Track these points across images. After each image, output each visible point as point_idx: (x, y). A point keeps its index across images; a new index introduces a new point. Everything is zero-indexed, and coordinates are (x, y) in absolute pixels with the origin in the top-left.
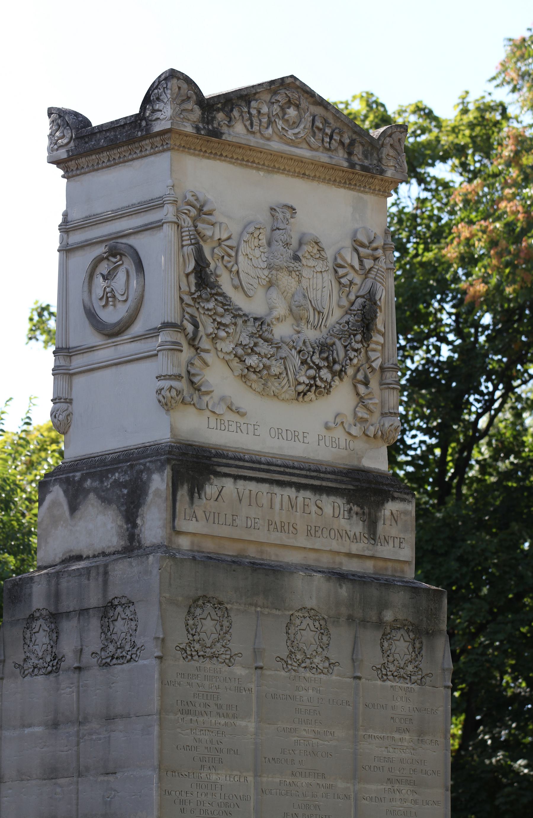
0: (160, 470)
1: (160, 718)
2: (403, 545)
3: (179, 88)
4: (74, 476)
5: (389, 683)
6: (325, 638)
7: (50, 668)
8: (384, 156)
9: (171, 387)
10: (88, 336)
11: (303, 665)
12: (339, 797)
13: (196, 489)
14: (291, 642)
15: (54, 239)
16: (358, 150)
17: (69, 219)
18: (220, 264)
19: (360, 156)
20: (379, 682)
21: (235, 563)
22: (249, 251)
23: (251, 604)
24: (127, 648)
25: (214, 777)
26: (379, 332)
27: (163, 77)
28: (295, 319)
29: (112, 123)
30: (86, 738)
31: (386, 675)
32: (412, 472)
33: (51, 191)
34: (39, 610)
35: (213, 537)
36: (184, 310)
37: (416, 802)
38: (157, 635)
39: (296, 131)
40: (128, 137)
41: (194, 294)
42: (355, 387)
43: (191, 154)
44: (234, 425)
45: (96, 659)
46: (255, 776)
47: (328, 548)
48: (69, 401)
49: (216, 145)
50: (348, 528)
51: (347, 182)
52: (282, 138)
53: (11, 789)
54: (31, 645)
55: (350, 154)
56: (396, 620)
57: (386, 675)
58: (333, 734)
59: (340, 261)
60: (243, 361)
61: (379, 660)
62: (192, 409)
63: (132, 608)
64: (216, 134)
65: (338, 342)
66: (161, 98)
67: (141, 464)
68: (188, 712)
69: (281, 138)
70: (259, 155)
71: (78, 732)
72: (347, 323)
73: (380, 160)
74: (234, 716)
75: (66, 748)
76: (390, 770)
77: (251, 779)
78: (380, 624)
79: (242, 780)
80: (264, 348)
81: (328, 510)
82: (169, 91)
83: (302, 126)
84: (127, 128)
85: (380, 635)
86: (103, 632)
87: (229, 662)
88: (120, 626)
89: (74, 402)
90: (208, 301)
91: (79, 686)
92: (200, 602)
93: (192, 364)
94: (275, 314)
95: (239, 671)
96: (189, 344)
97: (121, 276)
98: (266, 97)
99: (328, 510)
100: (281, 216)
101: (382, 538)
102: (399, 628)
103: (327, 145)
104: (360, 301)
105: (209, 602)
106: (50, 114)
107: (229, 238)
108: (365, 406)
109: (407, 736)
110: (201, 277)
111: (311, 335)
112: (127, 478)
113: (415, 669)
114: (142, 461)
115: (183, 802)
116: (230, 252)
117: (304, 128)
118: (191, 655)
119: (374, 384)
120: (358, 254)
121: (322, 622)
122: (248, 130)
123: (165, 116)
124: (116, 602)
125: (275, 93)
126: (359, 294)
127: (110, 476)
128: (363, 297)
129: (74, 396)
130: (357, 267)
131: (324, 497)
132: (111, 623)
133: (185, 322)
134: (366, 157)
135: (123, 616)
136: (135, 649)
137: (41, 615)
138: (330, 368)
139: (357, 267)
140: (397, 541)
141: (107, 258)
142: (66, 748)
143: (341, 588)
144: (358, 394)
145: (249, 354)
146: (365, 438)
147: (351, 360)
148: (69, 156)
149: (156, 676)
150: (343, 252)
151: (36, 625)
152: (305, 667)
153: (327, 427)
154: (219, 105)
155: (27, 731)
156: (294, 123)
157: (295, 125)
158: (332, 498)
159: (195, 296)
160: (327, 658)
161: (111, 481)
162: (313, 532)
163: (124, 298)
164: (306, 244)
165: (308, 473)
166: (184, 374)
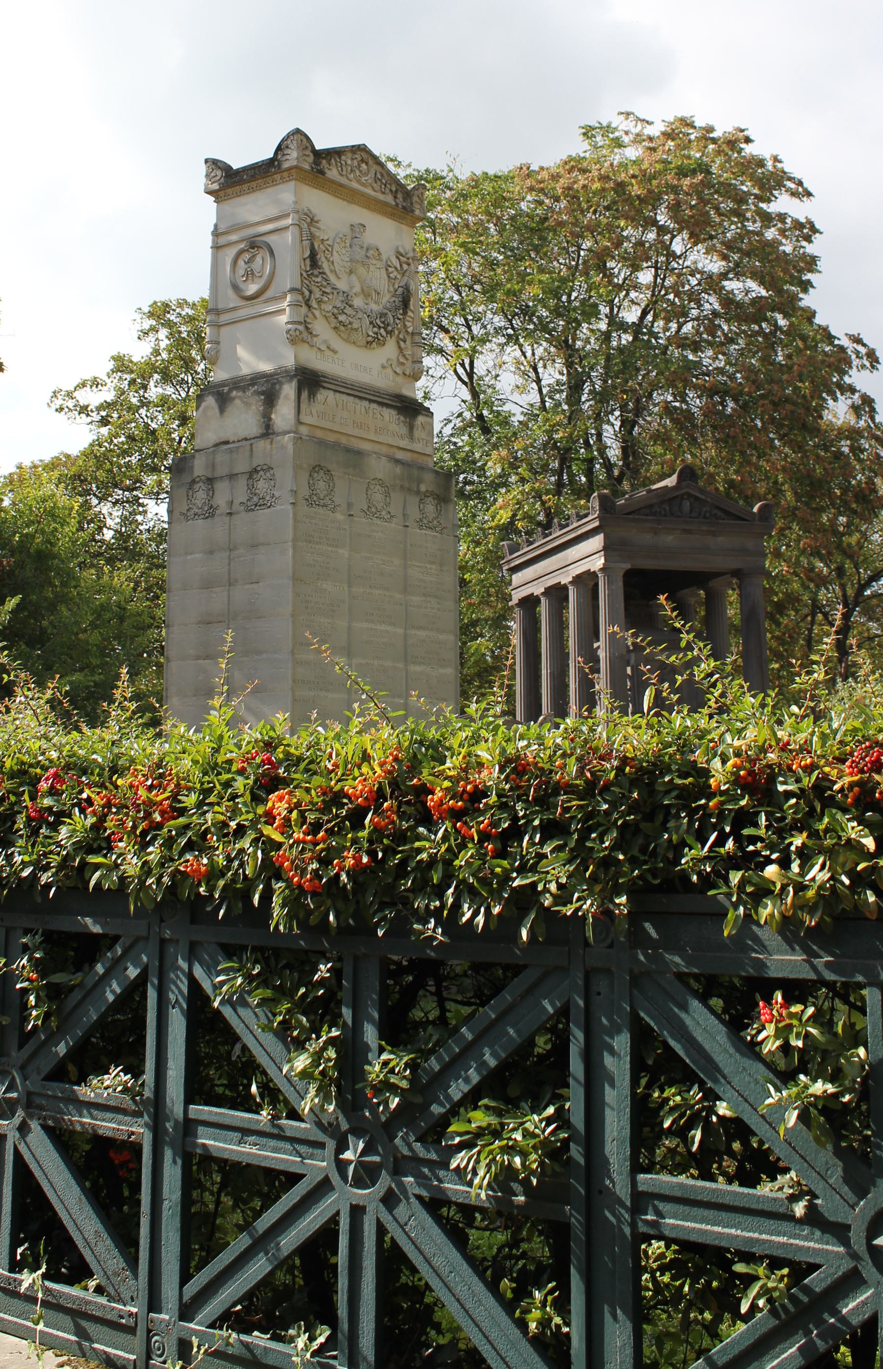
10: (232, 300)
13: (312, 395)
15: (209, 240)
16: (400, 196)
21: (336, 445)
25: (325, 586)
37: (439, 610)
46: (349, 586)
48: (218, 343)
51: (392, 216)
52: (359, 181)
55: (395, 197)
60: (336, 318)
61: (418, 516)
62: (306, 345)
64: (322, 172)
68: (310, 542)
74: (337, 547)
78: (418, 492)
80: (349, 311)
81: (387, 417)
90: (317, 276)
94: (354, 291)
95: (340, 517)
97: (259, 259)
98: (349, 155)
106: (206, 161)
108: (404, 356)
109: (434, 567)
111: (375, 307)
115: (307, 602)
116: (330, 249)
119: (408, 342)
123: (292, 157)
138: (385, 329)
144: (400, 347)
155: (189, 557)
157: (366, 174)
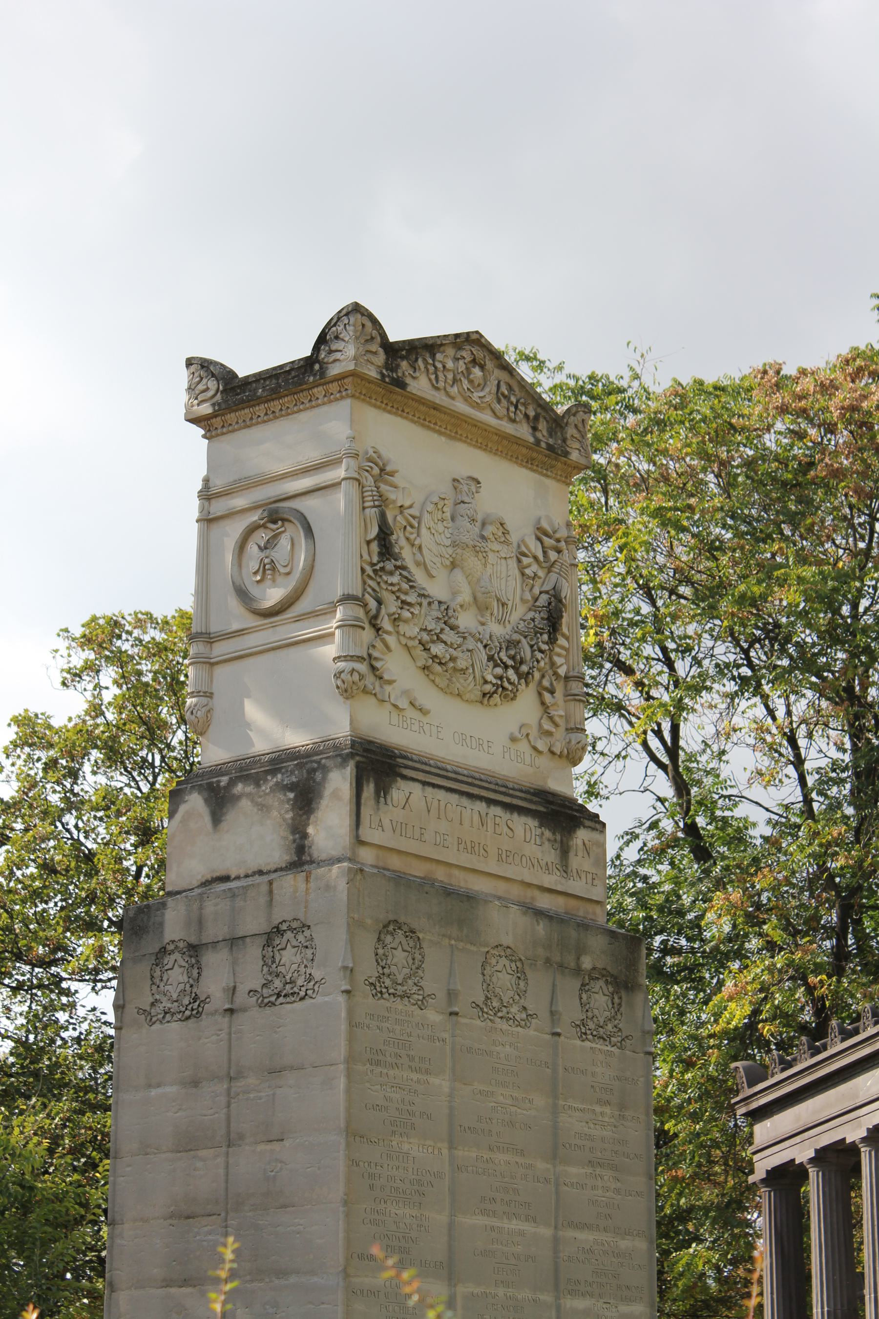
0: (343, 764)
1: (348, 1068)
2: (595, 882)
3: (363, 325)
4: (219, 782)
5: (587, 1044)
6: (522, 983)
7: (188, 1013)
8: (568, 436)
9: (353, 670)
10: (235, 616)
11: (500, 1014)
12: (539, 1181)
13: (382, 791)
14: (487, 985)
16: (542, 425)
17: (211, 484)
18: (401, 535)
19: (545, 433)
20: (578, 1042)
21: (425, 885)
22: (432, 524)
24: (300, 982)
25: (406, 1147)
26: (564, 635)
27: (344, 312)
28: (479, 608)
29: (274, 369)
30: (241, 1097)
31: (585, 1034)
33: (189, 455)
34: (173, 941)
35: (399, 852)
36: (364, 583)
37: (617, 1191)
38: (345, 964)
39: (481, 394)
40: (292, 384)
41: (375, 565)
42: (540, 694)
43: (370, 404)
44: (417, 723)
45: (255, 998)
46: (451, 1148)
47: (519, 879)
48: (209, 695)
49: (399, 398)
50: (540, 856)
51: (529, 463)
52: (467, 400)
53: (129, 1166)
54: (162, 984)
55: (535, 429)
56: (594, 969)
57: (585, 1034)
58: (531, 1101)
59: (524, 549)
60: (426, 650)
61: (578, 1015)
62: (372, 700)
63: (307, 933)
64: (400, 384)
65: (524, 640)
66: (341, 336)
67: (314, 761)
68: (378, 1063)
69: (466, 400)
70: (442, 416)
71: (229, 1090)
72: (533, 620)
73: (564, 440)
74: (427, 1072)
75: (210, 1112)
76: (591, 1150)
77: (445, 1151)
78: (578, 971)
79: (436, 1152)
80: (449, 636)
81: (519, 831)
82: (352, 328)
83: (487, 390)
84: (293, 374)
85: (577, 984)
86: (265, 964)
88: (289, 958)
89: (215, 696)
90: (391, 573)
91: (230, 1034)
92: (391, 928)
93: (374, 646)
95: (433, 1016)
96: (370, 623)
97: (284, 542)
98: (451, 351)
99: (519, 831)
100: (465, 488)
101: (575, 871)
102: (598, 979)
103: (512, 415)
104: (544, 598)
105: (400, 928)
106: (189, 363)
107: (411, 507)
108: (551, 718)
109: (607, 1110)
110: (385, 546)
111: (498, 630)
112: (294, 779)
113: (615, 1030)
114: (315, 758)
115: (371, 1176)
116: (414, 524)
117: (490, 393)
118: (381, 992)
119: (559, 694)
120: (542, 543)
121: (519, 964)
122: (433, 385)
123: (346, 355)
124: (284, 927)
125: (459, 348)
126: (543, 589)
127: (269, 778)
128: (547, 592)
129: (214, 690)
130: (541, 558)
131: (515, 815)
132: (276, 952)
133: (367, 596)
134: (551, 436)
135: (295, 943)
136: (312, 983)
137: (176, 947)
138: (516, 669)
139: (541, 558)
140: (590, 876)
141: (264, 526)
142: (210, 1112)
143: (538, 924)
144: (543, 703)
145: (433, 642)
146: (550, 755)
147: (538, 661)
148: (215, 411)
149: (343, 1014)
150: (527, 539)
151: (169, 960)
152: (501, 1018)
153: (513, 739)
154: (404, 353)
155: (154, 1092)
156: (479, 385)
158: (524, 819)
159: (378, 567)
160: (524, 1008)
161: (271, 784)
162: (504, 856)
163: (287, 570)
164: (491, 524)
165: (497, 788)
166: (365, 656)
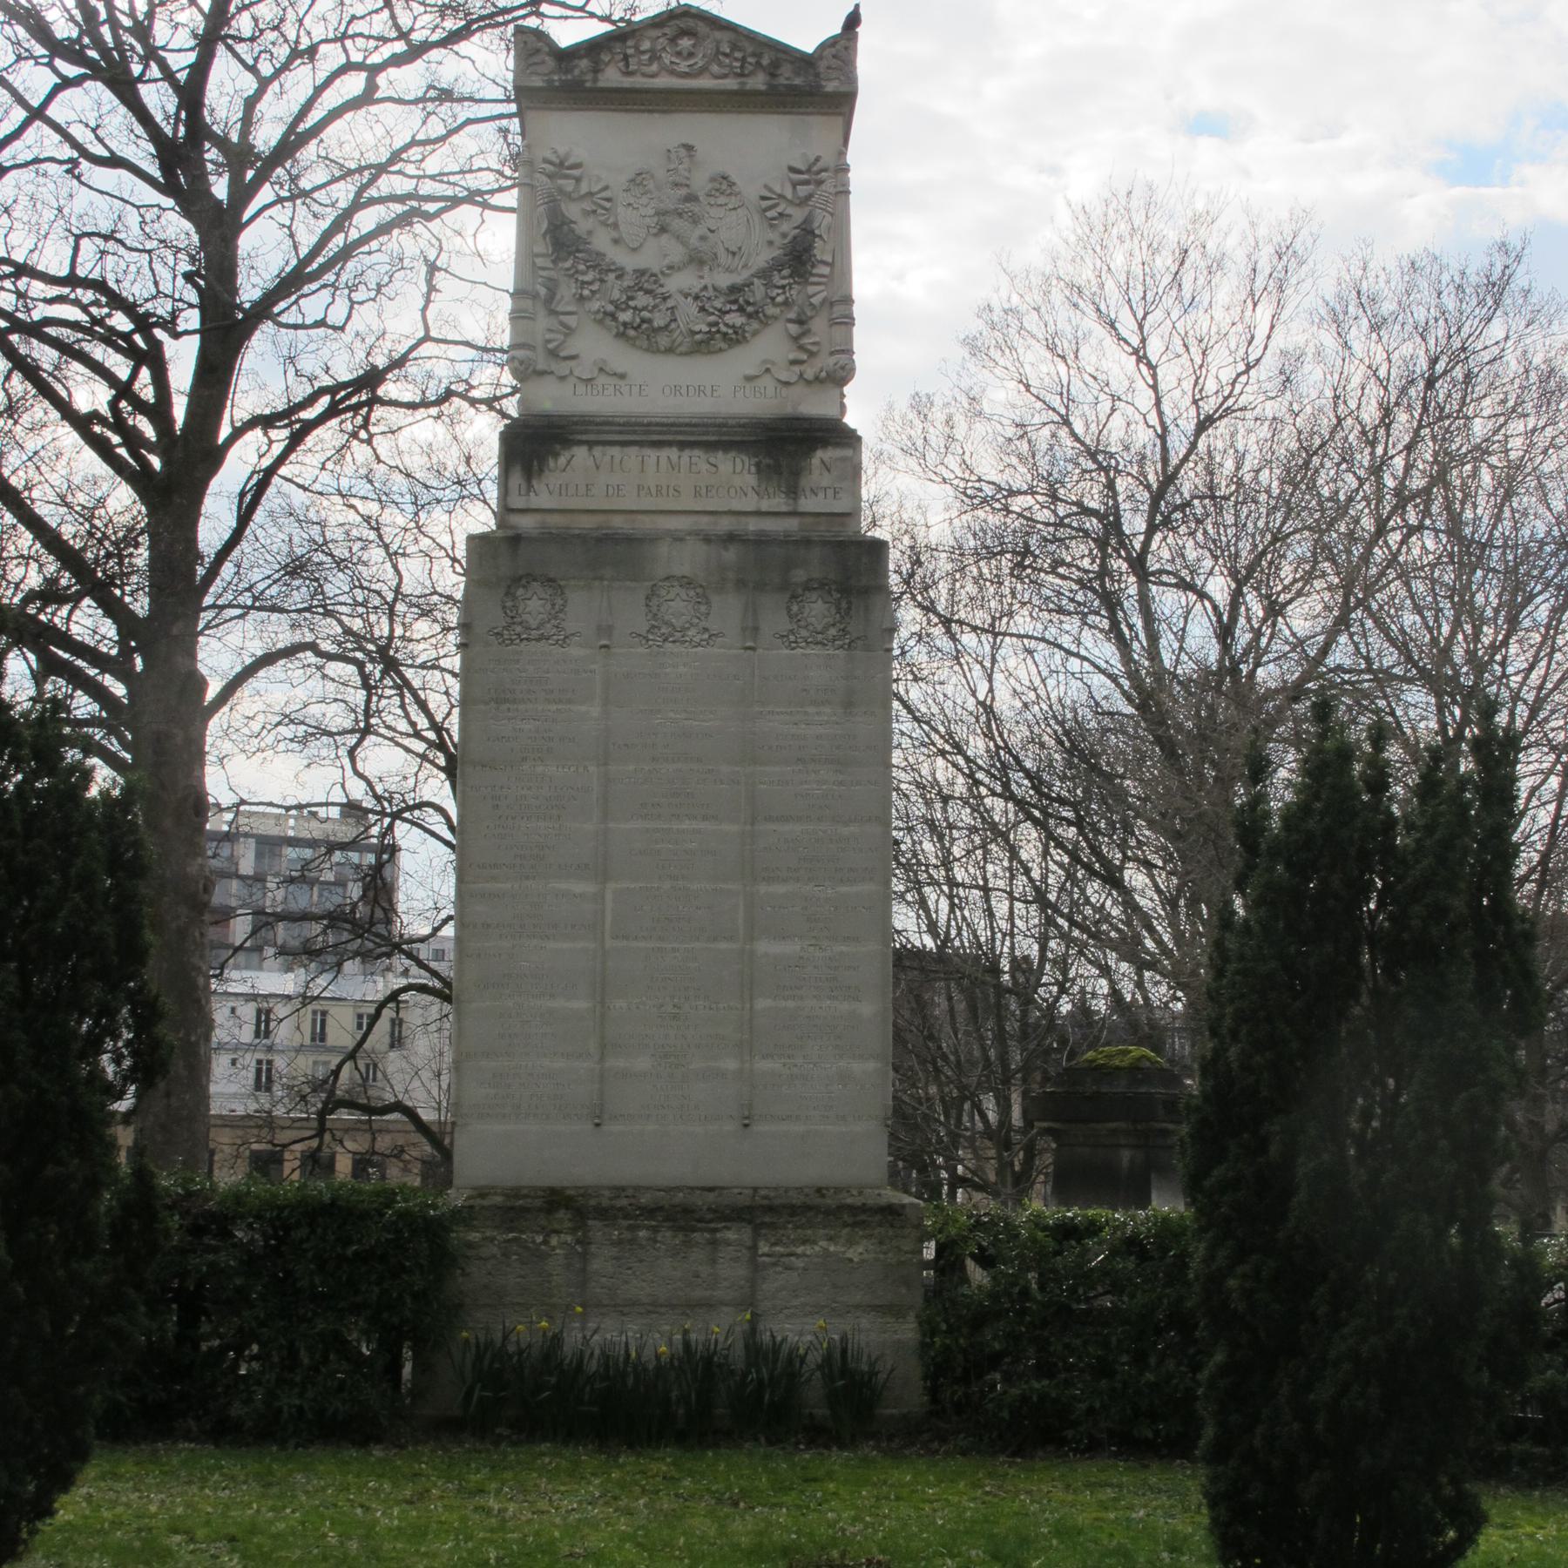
23: (595, 579)
32: (149, 368)
68: (506, 701)
74: (570, 701)
87: (563, 642)
92: (524, 582)
95: (575, 651)
109: (828, 710)
131: (720, 454)
140: (830, 492)
